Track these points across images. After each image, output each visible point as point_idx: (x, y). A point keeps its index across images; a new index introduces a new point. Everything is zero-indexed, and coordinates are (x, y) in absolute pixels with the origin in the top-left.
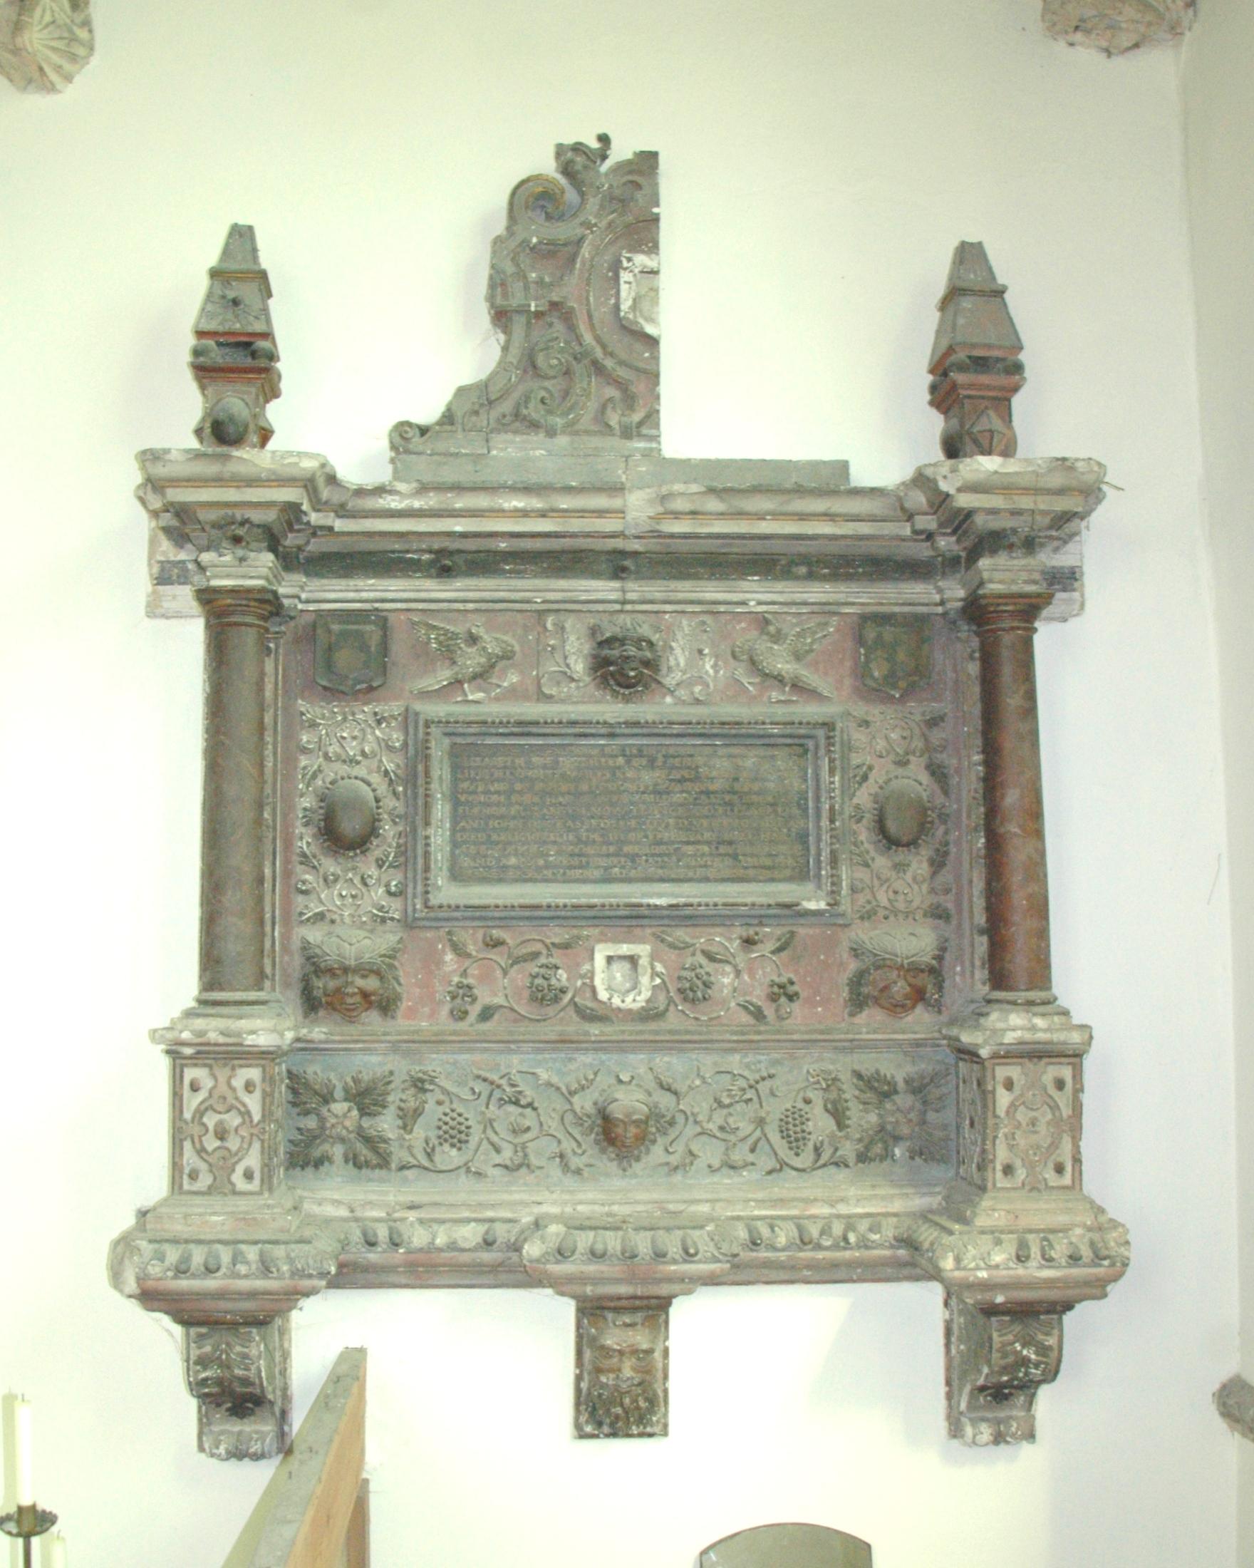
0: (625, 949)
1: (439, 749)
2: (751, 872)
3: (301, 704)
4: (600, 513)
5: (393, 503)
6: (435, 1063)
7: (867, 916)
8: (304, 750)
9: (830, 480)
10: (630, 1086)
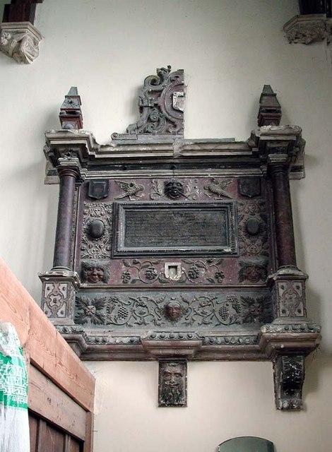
0: (173, 264)
1: (122, 212)
2: (210, 244)
3: (85, 203)
4: (167, 151)
5: (109, 149)
6: (119, 295)
7: (244, 254)
8: (85, 214)
9: (231, 142)
10: (174, 299)
